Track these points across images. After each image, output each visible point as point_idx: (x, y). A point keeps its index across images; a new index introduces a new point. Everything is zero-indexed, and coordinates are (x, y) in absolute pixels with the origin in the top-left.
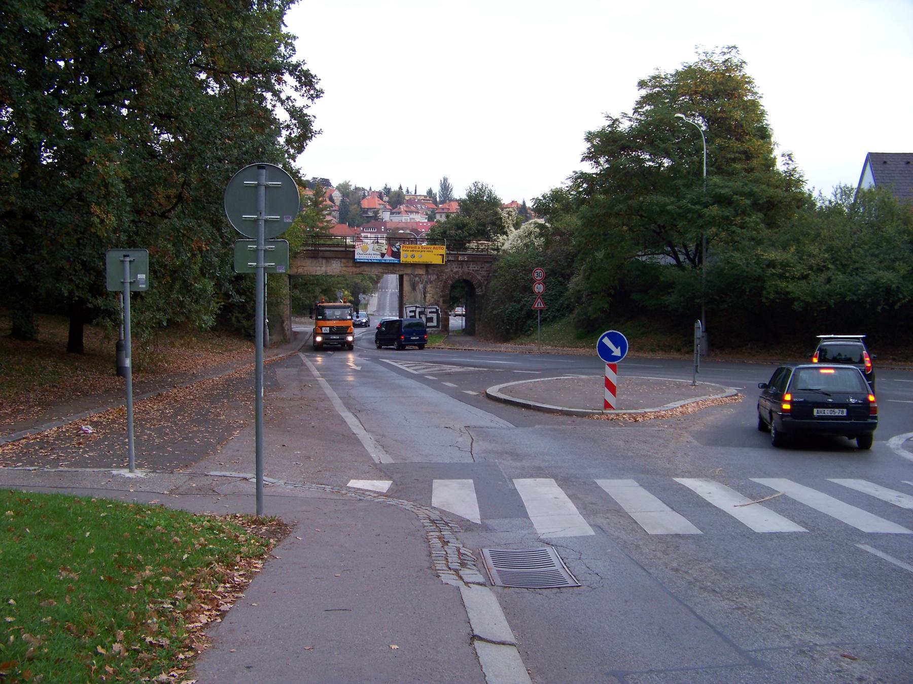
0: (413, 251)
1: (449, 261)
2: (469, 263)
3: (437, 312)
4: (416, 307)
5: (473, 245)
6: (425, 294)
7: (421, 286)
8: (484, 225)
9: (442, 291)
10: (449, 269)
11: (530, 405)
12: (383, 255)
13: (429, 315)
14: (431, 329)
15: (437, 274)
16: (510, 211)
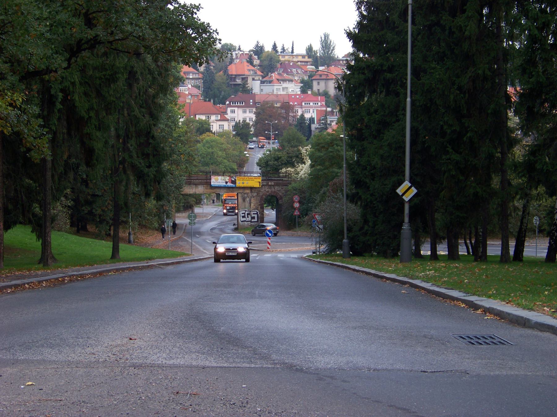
1: (263, 185)
2: (275, 186)
3: (257, 214)
4: (246, 211)
5: (284, 170)
6: (250, 203)
7: (248, 199)
8: (291, 157)
9: (259, 202)
10: (264, 190)
11: (528, 320)
12: (226, 183)
13: (253, 215)
15: (257, 193)
16: (307, 149)
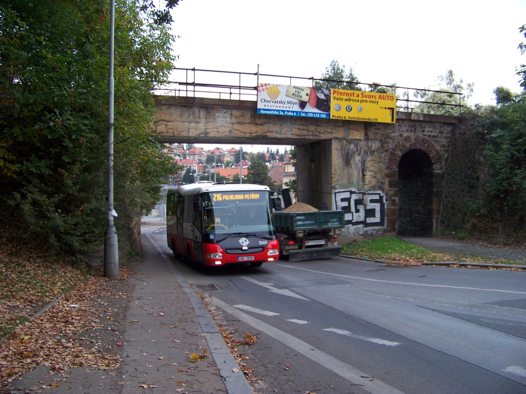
0: (349, 100)
9: (387, 168)
14: (371, 228)
